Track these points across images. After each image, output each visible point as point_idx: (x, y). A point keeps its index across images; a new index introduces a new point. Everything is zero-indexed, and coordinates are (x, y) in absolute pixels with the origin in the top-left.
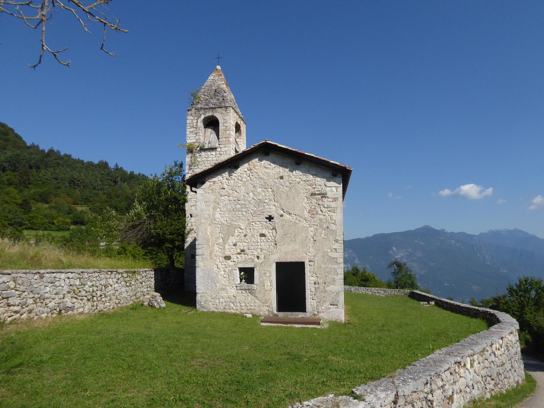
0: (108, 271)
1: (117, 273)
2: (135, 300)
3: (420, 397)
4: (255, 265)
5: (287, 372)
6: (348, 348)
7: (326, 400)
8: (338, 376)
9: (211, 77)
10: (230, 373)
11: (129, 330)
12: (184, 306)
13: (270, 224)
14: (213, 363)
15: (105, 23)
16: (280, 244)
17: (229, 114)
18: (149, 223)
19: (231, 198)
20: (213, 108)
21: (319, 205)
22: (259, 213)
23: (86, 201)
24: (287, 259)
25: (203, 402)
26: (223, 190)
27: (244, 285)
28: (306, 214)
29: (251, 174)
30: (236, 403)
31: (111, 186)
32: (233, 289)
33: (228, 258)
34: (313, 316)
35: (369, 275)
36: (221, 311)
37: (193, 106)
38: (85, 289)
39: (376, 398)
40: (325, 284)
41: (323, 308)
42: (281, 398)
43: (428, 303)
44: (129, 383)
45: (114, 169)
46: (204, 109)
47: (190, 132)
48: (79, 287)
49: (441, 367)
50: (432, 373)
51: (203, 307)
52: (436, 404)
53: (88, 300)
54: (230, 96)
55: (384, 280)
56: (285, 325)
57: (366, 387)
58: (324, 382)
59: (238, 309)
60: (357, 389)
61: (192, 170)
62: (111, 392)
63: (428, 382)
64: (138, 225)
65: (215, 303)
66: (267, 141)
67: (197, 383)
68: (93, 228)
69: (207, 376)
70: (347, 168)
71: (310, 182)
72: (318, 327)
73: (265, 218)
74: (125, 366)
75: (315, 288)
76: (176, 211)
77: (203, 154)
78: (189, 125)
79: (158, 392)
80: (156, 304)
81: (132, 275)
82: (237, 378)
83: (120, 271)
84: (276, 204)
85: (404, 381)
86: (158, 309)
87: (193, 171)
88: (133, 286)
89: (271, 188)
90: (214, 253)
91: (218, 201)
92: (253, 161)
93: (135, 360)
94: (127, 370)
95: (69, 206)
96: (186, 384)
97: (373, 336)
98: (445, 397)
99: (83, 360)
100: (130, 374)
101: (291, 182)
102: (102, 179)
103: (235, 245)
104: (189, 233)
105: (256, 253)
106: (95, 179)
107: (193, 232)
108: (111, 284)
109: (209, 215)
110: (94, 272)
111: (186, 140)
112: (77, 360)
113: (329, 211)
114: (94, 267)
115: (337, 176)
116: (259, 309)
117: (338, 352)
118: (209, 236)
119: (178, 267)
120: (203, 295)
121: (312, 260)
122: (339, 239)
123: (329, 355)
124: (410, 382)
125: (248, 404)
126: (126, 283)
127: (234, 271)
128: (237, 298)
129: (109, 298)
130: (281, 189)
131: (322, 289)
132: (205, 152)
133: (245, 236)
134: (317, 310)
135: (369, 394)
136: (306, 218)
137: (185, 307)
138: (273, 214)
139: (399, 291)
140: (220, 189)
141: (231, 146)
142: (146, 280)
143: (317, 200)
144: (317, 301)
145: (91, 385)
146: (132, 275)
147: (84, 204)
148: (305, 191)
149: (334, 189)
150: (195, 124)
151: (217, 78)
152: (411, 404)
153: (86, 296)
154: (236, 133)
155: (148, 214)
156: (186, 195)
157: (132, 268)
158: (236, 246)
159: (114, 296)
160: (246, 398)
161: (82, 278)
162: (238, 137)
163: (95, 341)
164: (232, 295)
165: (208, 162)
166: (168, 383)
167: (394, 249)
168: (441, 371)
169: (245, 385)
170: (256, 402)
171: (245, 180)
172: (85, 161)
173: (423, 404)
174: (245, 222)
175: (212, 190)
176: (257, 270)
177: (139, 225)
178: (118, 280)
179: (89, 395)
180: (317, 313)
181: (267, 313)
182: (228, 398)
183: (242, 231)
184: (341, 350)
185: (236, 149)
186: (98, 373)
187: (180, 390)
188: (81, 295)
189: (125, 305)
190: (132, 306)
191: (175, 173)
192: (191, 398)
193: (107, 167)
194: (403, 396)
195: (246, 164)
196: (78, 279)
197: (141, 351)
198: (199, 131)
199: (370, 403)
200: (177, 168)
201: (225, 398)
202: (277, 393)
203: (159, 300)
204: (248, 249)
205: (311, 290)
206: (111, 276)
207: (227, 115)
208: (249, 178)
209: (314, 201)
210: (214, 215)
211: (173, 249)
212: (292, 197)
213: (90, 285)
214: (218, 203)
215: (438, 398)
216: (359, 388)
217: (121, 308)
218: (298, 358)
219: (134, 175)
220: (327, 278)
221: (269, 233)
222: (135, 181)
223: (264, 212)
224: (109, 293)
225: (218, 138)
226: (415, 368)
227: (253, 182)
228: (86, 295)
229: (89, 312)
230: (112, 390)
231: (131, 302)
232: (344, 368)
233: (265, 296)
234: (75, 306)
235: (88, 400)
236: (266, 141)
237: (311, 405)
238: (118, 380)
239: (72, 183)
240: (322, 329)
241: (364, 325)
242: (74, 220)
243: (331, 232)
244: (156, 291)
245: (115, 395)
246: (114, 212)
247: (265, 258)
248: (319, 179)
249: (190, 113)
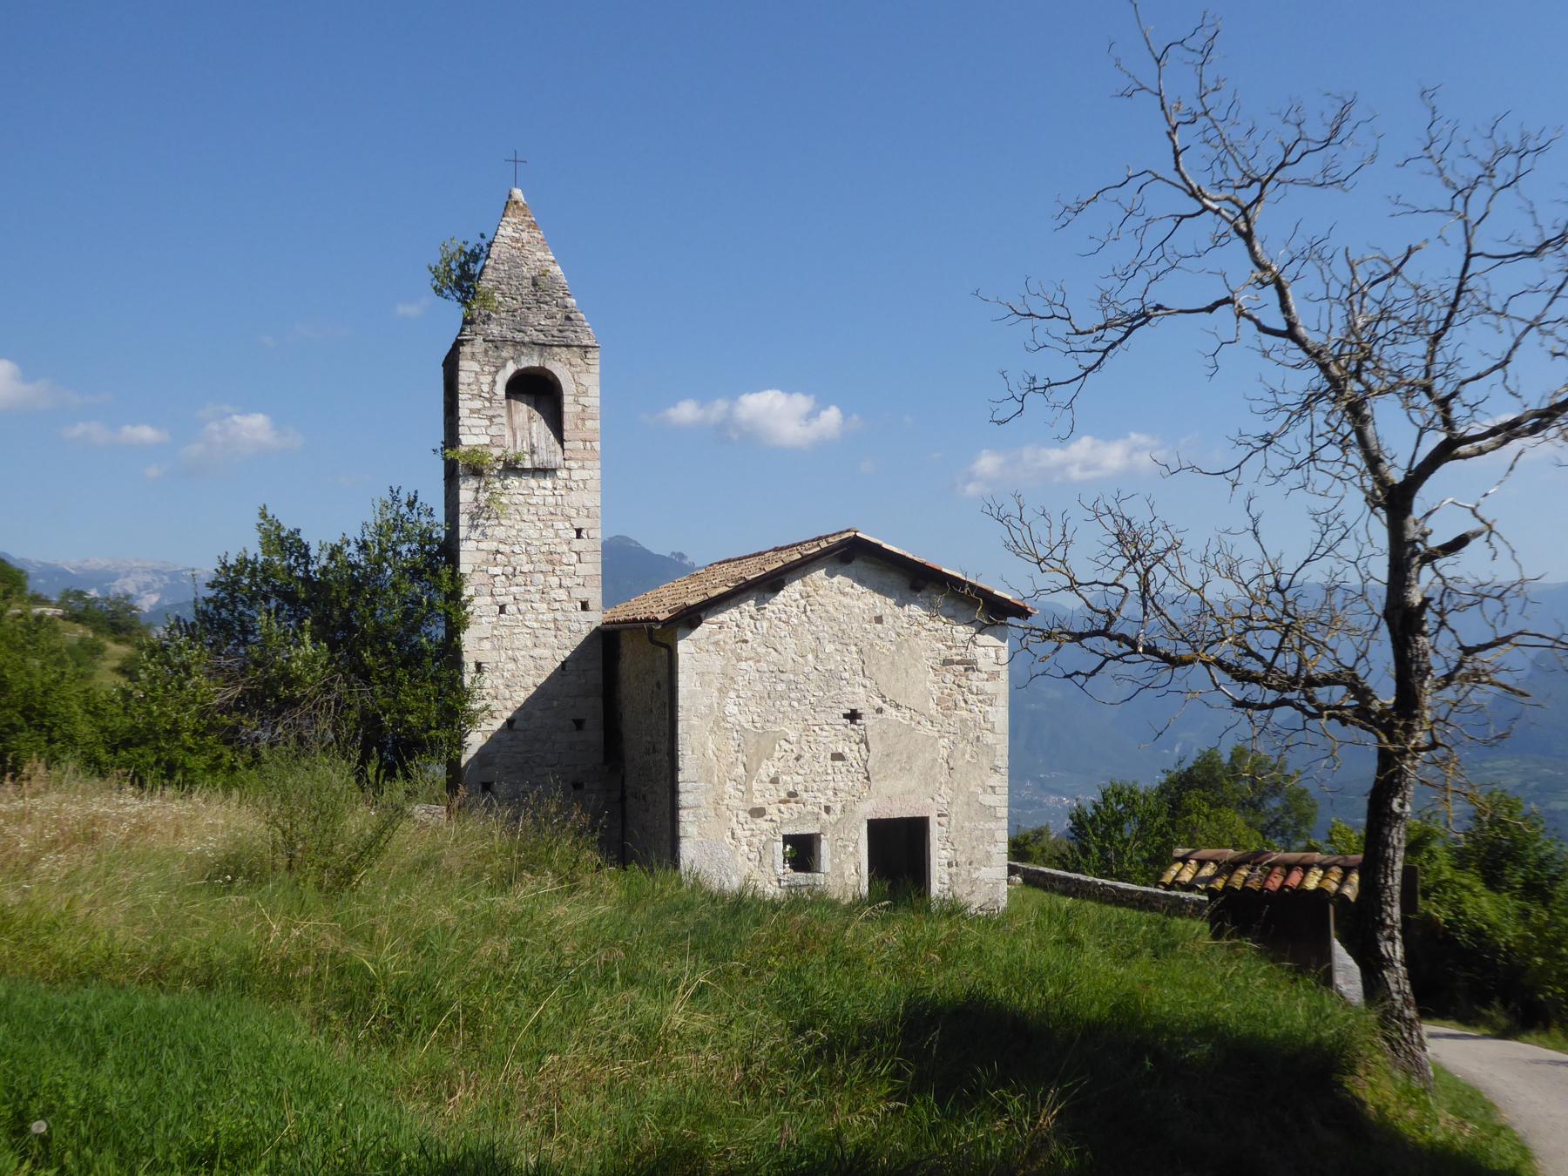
13: (854, 730)
19: (763, 666)
20: (544, 345)
21: (959, 686)
22: (830, 703)
26: (744, 645)
33: (758, 812)
46: (515, 343)
47: (472, 411)
66: (858, 534)
75: (950, 874)
77: (513, 482)
89: (856, 645)
90: (726, 802)
91: (730, 671)
103: (774, 781)
105: (823, 801)
109: (710, 707)
113: (980, 701)
118: (711, 760)
121: (946, 812)
132: (520, 476)
133: (797, 759)
136: (932, 716)
138: (861, 707)
148: (929, 654)
150: (486, 388)
151: (525, 235)
171: (796, 621)
183: (791, 746)
207: (588, 372)
208: (803, 617)
220: (976, 850)
225: (561, 441)
227: (815, 628)
243: (985, 749)
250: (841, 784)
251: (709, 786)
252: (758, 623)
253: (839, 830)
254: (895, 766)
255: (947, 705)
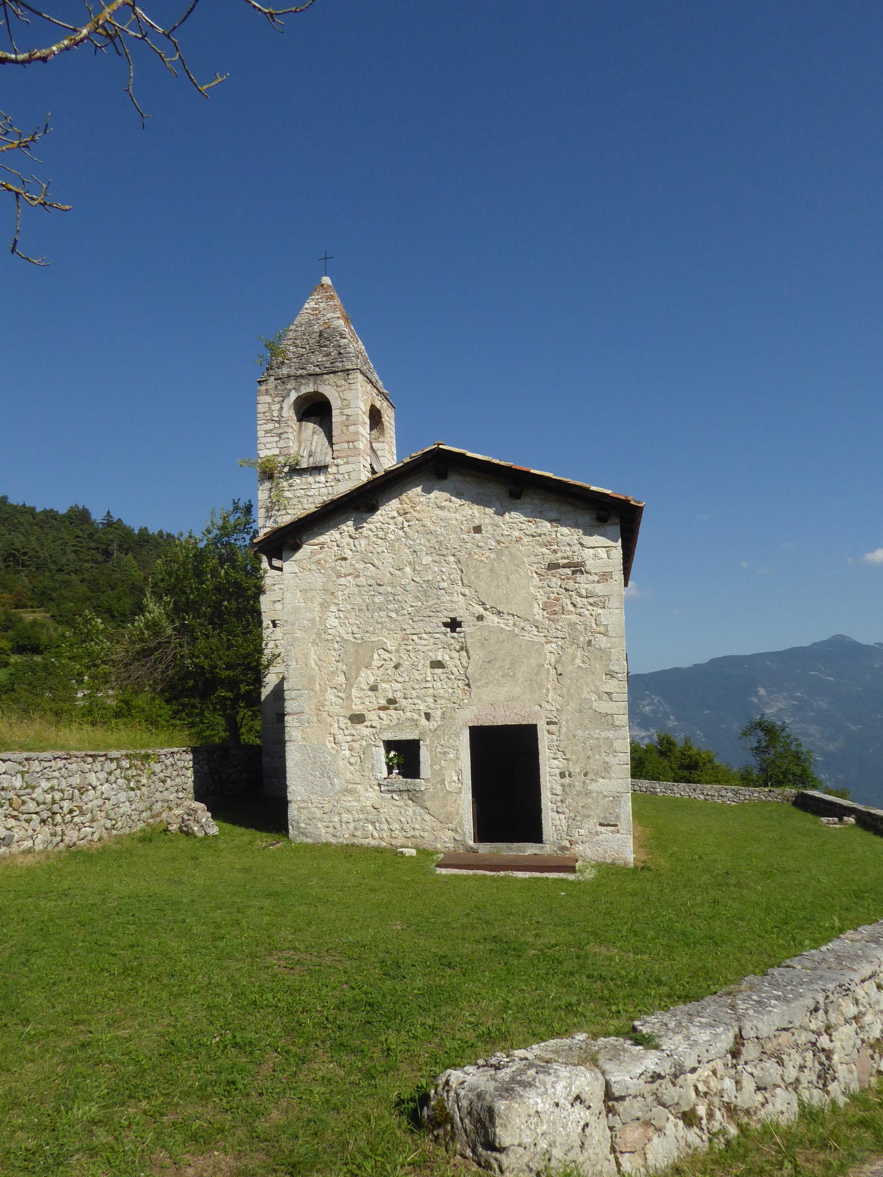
0: (86, 755)
1: (106, 760)
2: (150, 821)
3: (799, 1042)
4: (420, 733)
5: (485, 981)
6: (637, 927)
7: (567, 1047)
8: (606, 992)
9: (310, 304)
10: (353, 985)
11: (131, 886)
12: (262, 831)
13: (453, 638)
14: (317, 960)
15: (17, 194)
16: (478, 684)
17: (353, 387)
18: (180, 644)
19: (362, 580)
20: (317, 375)
21: (567, 590)
23: (43, 598)
24: (494, 718)
25: (285, 1049)
26: (343, 563)
27: (399, 781)
28: (538, 613)
29: (406, 524)
30: (362, 1051)
31: (96, 562)
32: (371, 790)
33: (357, 719)
34: (559, 852)
35: (699, 754)
36: (345, 842)
37: (271, 372)
38: (34, 796)
39: (687, 1043)
40: (586, 775)
41: (582, 832)
42: (467, 1042)
43: (841, 820)
44: (122, 1006)
45: (103, 524)
46: (297, 377)
47: (266, 432)
48: (22, 792)
49: (854, 970)
50: (831, 986)
51: (304, 834)
52: (840, 1058)
53: (43, 821)
54: (355, 345)
55: (736, 768)
56: (492, 873)
57: (666, 1018)
58: (570, 1004)
59: (385, 837)
60: (646, 1022)
61: (272, 520)
62: (81, 1027)
63: (819, 1006)
64: (155, 648)
65: (331, 824)
66: (441, 446)
67: (276, 1007)
68: (53, 660)
69: (300, 991)
70: (632, 502)
71: (543, 536)
72: (571, 877)
73: (441, 625)
74: (116, 969)
75: (563, 785)
76: (239, 614)
77: (297, 480)
78: (262, 415)
79: (186, 1026)
80: (196, 828)
81: (142, 764)
82: (369, 995)
83: (114, 754)
84: (467, 591)
85: (759, 1002)
86: (201, 840)
87: (275, 522)
88: (143, 789)
89: (454, 555)
90: (327, 708)
92: (409, 492)
93: (138, 956)
94: (120, 978)
95: (5, 613)
96: (250, 1009)
97: (699, 898)
98: (863, 1041)
99: (24, 956)
100: (127, 987)
101: (499, 538)
102: (77, 548)
103: (373, 688)
104: (270, 663)
106: (62, 549)
107: (280, 661)
108: (94, 784)
110: (55, 759)
111: (255, 450)
112: (11, 955)
113: (591, 604)
114: (54, 747)
115: (609, 522)
116: (433, 837)
117: (611, 935)
118: (313, 669)
119: (251, 742)
120: (302, 805)
121: (555, 720)
122: (618, 671)
123: (588, 943)
124: (774, 1007)
125: (388, 1054)
126: (129, 781)
127: (374, 749)
128: (382, 810)
129: (89, 815)
130: (476, 557)
131: (579, 788)
133: (396, 667)
134: (568, 837)
135: (671, 1034)
136: (537, 621)
137: (264, 834)
138: (461, 614)
139: (770, 791)
140: (336, 560)
141: (362, 460)
142: (175, 773)
143: (563, 580)
144: (567, 816)
145: (37, 1010)
146: (142, 764)
147: (38, 607)
149: (602, 553)
150: (276, 414)
151: (322, 305)
152: (776, 1057)
153: (37, 813)
154: (371, 429)
155: (177, 624)
156: (262, 578)
157: (143, 747)
158: (376, 690)
159: (101, 811)
160: (386, 1040)
161: (27, 772)
162: (377, 439)
163: (54, 913)
164: (369, 803)
165: (309, 499)
166: (208, 1006)
167: (762, 691)
168: (852, 980)
169: (386, 1010)
170: (408, 1051)
171: (393, 537)
172: (38, 510)
173: (807, 1059)
174: (395, 635)
175: (318, 562)
176: (426, 745)
177: (155, 649)
178: (110, 775)
179: (32, 1033)
180: (568, 846)
181: (451, 845)
182: (344, 1040)
183: (389, 655)
184: (619, 931)
185: (372, 468)
186: (54, 984)
187: (236, 1022)
188: (26, 811)
189: (128, 832)
190: (142, 834)
191: (235, 527)
192: (260, 1040)
193: (87, 521)
194: (756, 1040)
195: (394, 501)
196: (19, 775)
197: (155, 935)
198: (285, 429)
199: (672, 1055)
200: (238, 515)
201: (338, 1040)
202: (459, 1030)
203: (204, 820)
204: (405, 698)
205: (554, 792)
206: (94, 767)
207: (350, 389)
208: (401, 533)
209: (555, 581)
210: (323, 620)
211: (235, 701)
212: (503, 573)
213: (46, 788)
214: (333, 593)
215: (844, 1044)
216: (648, 1019)
217: (119, 840)
218: (514, 950)
219: (148, 535)
220: (591, 761)
221: (452, 658)
222: (151, 550)
223: (438, 609)
224: (90, 805)
225: (331, 444)
226: (789, 973)
227: (412, 543)
228: (38, 810)
229: (46, 848)
230: (82, 1022)
231: (141, 825)
232: (623, 973)
233: (445, 805)
234: (14, 836)
235: (30, 1043)
236: (439, 444)
237: (530, 1058)
238: (100, 1000)
239: (11, 559)
240: (579, 883)
241: (681, 873)
242: (17, 642)
244: (198, 798)
245: (91, 1032)
246: (100, 620)
247: (443, 717)
248: (565, 530)
249: (263, 388)
250: (441, 691)
251: (312, 693)
252: (356, 541)
253: (439, 737)
254: (497, 673)
255: (552, 609)
